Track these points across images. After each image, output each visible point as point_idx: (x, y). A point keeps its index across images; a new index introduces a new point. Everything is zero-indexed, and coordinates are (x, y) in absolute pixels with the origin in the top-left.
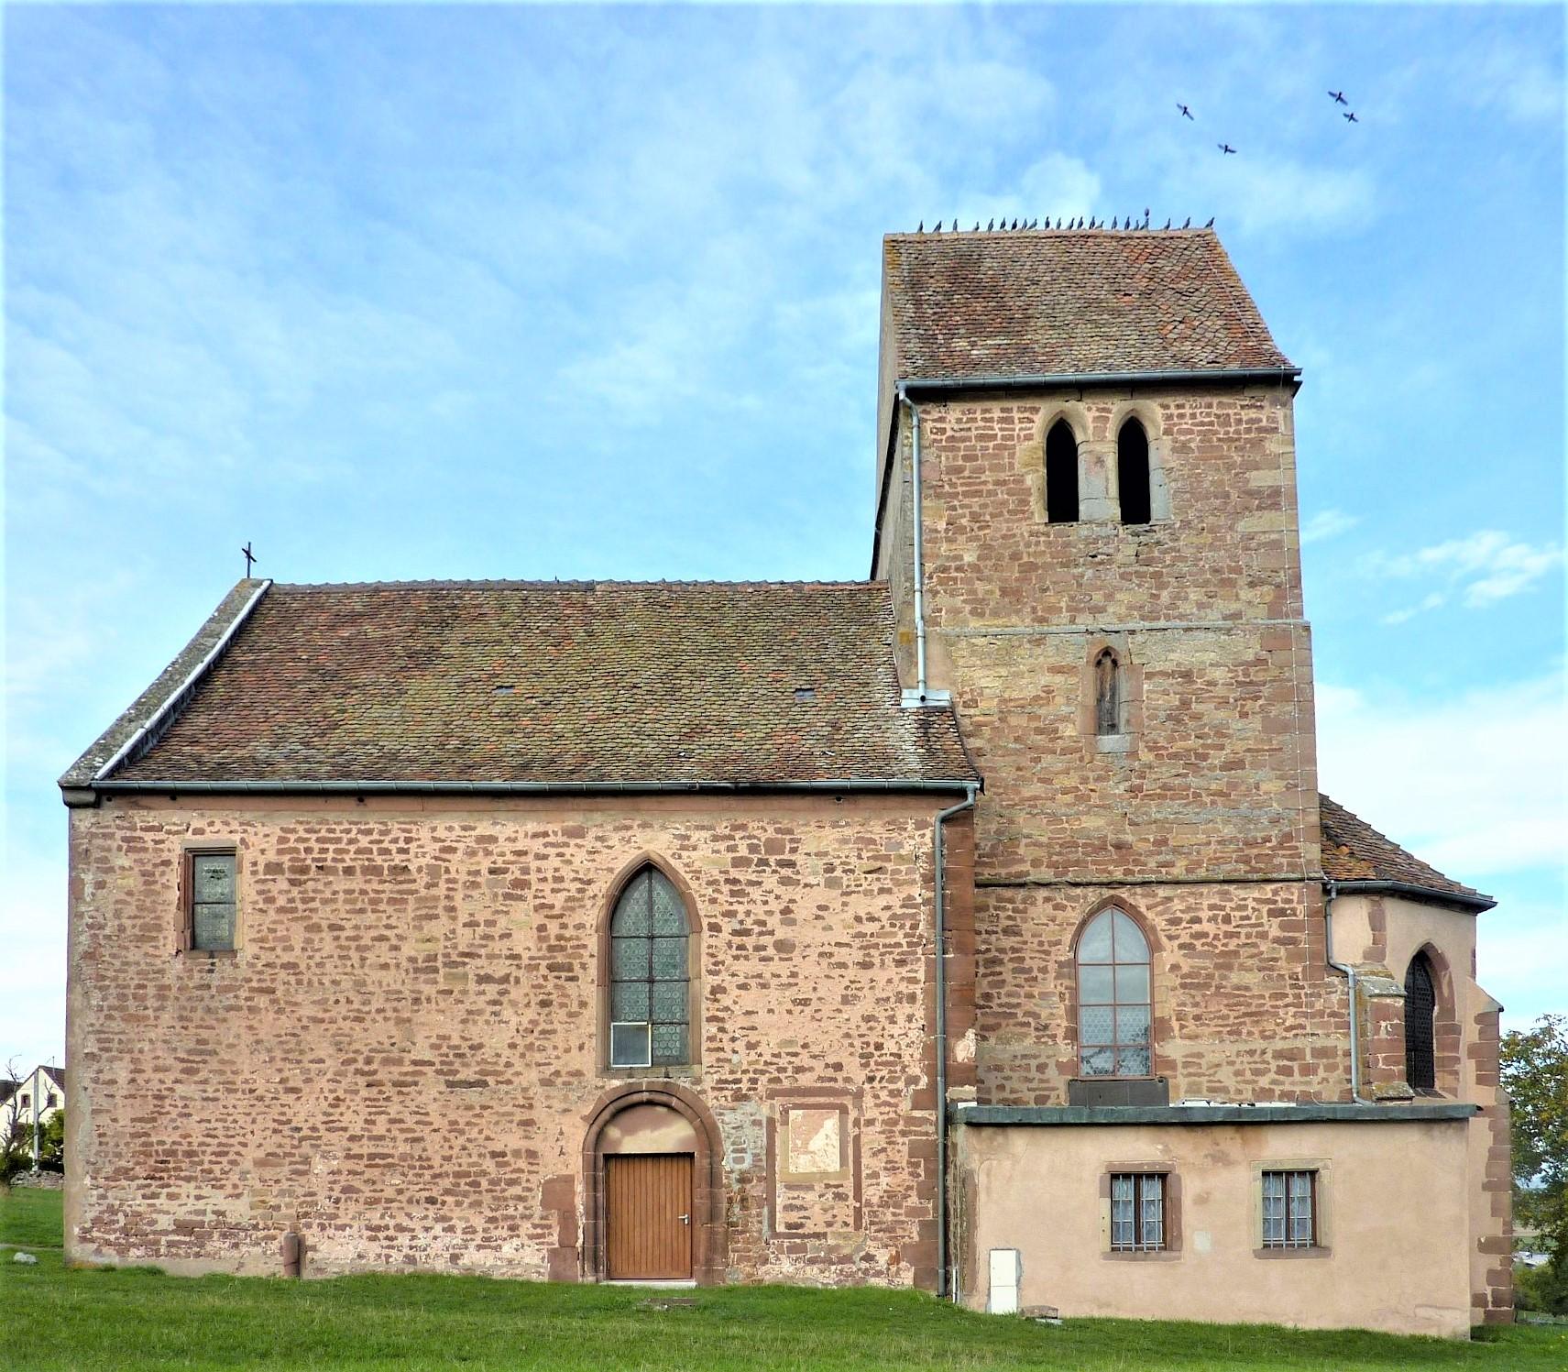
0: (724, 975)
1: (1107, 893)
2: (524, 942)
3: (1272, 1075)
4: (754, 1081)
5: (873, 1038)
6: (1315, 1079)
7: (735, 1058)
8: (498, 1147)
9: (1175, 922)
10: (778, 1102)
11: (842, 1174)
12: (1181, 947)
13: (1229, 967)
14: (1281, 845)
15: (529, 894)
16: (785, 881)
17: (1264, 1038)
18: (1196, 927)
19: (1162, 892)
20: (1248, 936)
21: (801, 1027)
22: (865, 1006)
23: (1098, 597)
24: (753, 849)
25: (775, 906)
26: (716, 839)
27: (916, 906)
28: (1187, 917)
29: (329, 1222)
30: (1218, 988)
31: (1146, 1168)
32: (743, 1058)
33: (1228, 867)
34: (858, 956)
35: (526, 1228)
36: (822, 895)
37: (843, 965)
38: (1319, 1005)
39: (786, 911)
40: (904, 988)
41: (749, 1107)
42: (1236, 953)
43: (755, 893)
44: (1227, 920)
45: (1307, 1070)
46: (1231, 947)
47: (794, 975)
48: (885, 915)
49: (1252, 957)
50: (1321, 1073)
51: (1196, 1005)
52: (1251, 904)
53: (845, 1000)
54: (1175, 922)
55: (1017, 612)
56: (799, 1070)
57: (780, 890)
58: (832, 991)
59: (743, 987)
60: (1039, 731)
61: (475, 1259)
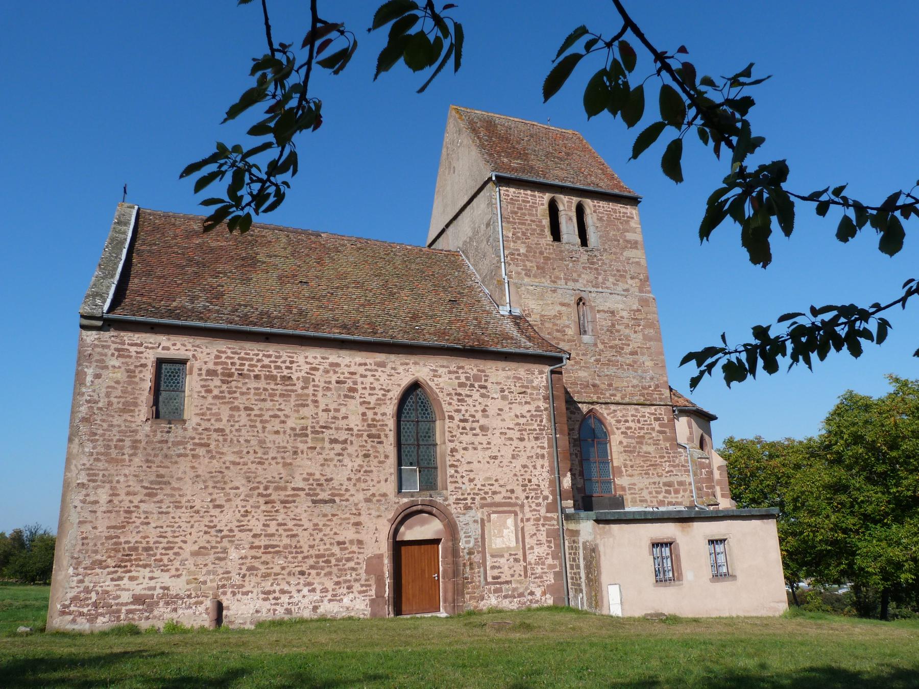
0: (456, 443)
2: (355, 421)
3: (663, 494)
4: (473, 499)
5: (527, 477)
6: (680, 496)
7: (464, 487)
8: (340, 538)
10: (485, 509)
11: (517, 548)
12: (622, 433)
13: (641, 443)
14: (655, 390)
15: (357, 395)
16: (483, 396)
17: (659, 476)
19: (613, 407)
21: (494, 471)
23: (575, 275)
24: (467, 378)
25: (479, 408)
26: (450, 372)
27: (541, 411)
28: (623, 419)
31: (665, 540)
33: (636, 398)
34: (518, 435)
35: (357, 587)
37: (511, 439)
38: (677, 462)
39: (484, 411)
40: (539, 451)
41: (472, 513)
42: (643, 437)
44: (639, 421)
47: (489, 443)
48: (528, 415)
50: (682, 493)
51: (631, 460)
52: (647, 415)
53: (513, 457)
54: (618, 421)
55: (544, 277)
56: (494, 493)
57: (480, 400)
58: (507, 452)
59: (465, 449)
60: (558, 331)
61: (328, 608)
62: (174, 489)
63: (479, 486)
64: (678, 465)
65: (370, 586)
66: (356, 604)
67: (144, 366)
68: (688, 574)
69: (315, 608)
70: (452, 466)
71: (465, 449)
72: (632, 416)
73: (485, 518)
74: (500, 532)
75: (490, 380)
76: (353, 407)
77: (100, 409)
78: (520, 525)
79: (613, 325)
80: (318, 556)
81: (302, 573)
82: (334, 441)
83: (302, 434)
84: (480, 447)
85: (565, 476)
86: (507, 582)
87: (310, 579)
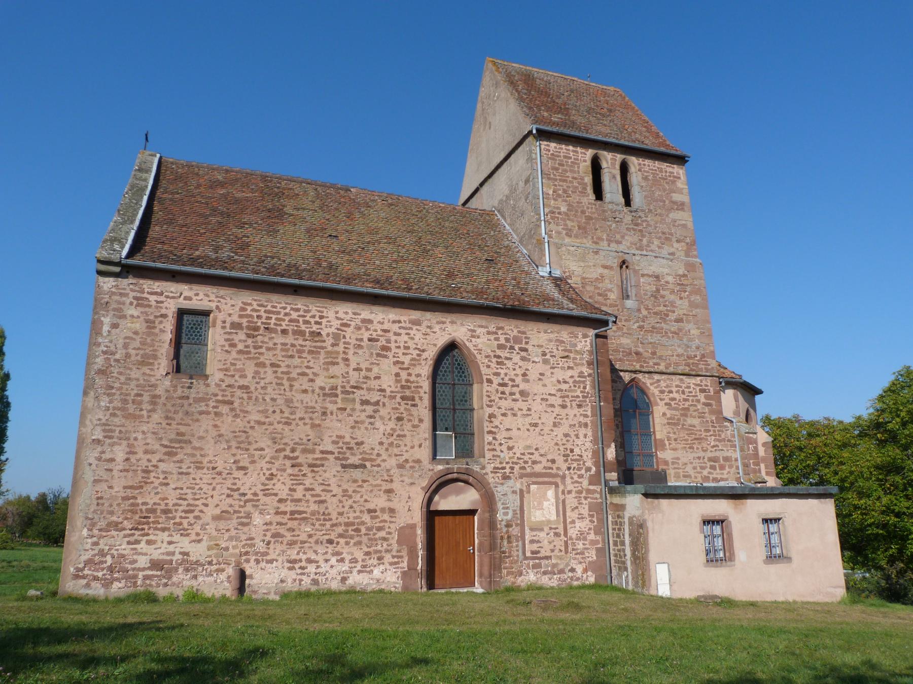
0: (494, 408)
1: (634, 376)
2: (388, 382)
4: (512, 468)
5: (569, 446)
6: (725, 472)
7: (502, 455)
8: (371, 506)
9: (662, 392)
10: (525, 480)
11: (557, 521)
15: (390, 354)
17: (704, 451)
18: (671, 395)
19: (656, 377)
20: (693, 401)
21: (534, 439)
22: (564, 428)
23: (618, 237)
24: (507, 340)
27: (585, 377)
28: (667, 390)
29: (262, 558)
30: (683, 425)
31: (717, 518)
32: (506, 455)
34: (560, 401)
35: (388, 558)
36: (541, 368)
38: (723, 436)
39: (524, 375)
41: (510, 483)
42: (688, 409)
43: (509, 364)
44: (683, 392)
45: (722, 468)
46: (686, 406)
47: (529, 410)
48: (571, 381)
49: (695, 411)
51: (675, 433)
52: (692, 386)
54: (662, 392)
55: (586, 237)
56: (534, 462)
58: (548, 419)
59: (504, 415)
61: (357, 579)
62: (195, 448)
63: (518, 455)
64: (724, 440)
65: (401, 557)
66: (387, 576)
67: (164, 316)
68: (741, 555)
69: (344, 579)
70: (490, 432)
71: (504, 415)
72: (677, 386)
73: (524, 489)
74: (540, 503)
75: (531, 343)
76: (386, 366)
77: (117, 361)
78: (561, 497)
79: (658, 290)
80: (347, 524)
81: (330, 542)
82: (365, 402)
83: (331, 393)
84: (519, 413)
85: (609, 446)
86: (547, 558)
87: (338, 549)
